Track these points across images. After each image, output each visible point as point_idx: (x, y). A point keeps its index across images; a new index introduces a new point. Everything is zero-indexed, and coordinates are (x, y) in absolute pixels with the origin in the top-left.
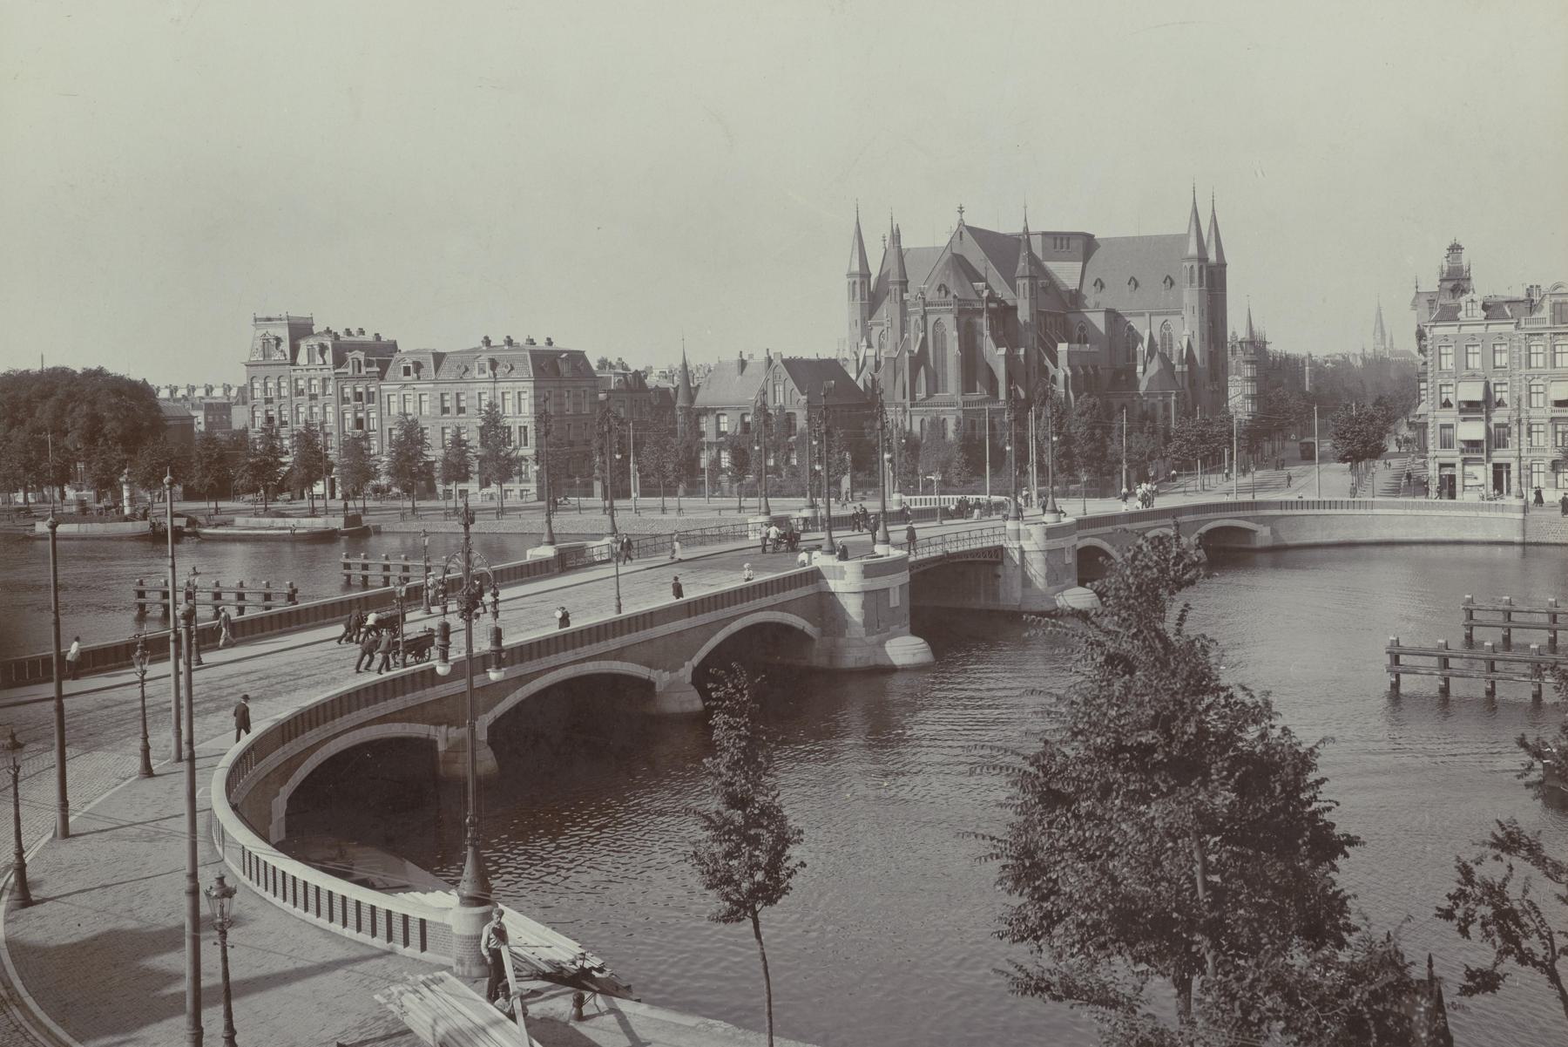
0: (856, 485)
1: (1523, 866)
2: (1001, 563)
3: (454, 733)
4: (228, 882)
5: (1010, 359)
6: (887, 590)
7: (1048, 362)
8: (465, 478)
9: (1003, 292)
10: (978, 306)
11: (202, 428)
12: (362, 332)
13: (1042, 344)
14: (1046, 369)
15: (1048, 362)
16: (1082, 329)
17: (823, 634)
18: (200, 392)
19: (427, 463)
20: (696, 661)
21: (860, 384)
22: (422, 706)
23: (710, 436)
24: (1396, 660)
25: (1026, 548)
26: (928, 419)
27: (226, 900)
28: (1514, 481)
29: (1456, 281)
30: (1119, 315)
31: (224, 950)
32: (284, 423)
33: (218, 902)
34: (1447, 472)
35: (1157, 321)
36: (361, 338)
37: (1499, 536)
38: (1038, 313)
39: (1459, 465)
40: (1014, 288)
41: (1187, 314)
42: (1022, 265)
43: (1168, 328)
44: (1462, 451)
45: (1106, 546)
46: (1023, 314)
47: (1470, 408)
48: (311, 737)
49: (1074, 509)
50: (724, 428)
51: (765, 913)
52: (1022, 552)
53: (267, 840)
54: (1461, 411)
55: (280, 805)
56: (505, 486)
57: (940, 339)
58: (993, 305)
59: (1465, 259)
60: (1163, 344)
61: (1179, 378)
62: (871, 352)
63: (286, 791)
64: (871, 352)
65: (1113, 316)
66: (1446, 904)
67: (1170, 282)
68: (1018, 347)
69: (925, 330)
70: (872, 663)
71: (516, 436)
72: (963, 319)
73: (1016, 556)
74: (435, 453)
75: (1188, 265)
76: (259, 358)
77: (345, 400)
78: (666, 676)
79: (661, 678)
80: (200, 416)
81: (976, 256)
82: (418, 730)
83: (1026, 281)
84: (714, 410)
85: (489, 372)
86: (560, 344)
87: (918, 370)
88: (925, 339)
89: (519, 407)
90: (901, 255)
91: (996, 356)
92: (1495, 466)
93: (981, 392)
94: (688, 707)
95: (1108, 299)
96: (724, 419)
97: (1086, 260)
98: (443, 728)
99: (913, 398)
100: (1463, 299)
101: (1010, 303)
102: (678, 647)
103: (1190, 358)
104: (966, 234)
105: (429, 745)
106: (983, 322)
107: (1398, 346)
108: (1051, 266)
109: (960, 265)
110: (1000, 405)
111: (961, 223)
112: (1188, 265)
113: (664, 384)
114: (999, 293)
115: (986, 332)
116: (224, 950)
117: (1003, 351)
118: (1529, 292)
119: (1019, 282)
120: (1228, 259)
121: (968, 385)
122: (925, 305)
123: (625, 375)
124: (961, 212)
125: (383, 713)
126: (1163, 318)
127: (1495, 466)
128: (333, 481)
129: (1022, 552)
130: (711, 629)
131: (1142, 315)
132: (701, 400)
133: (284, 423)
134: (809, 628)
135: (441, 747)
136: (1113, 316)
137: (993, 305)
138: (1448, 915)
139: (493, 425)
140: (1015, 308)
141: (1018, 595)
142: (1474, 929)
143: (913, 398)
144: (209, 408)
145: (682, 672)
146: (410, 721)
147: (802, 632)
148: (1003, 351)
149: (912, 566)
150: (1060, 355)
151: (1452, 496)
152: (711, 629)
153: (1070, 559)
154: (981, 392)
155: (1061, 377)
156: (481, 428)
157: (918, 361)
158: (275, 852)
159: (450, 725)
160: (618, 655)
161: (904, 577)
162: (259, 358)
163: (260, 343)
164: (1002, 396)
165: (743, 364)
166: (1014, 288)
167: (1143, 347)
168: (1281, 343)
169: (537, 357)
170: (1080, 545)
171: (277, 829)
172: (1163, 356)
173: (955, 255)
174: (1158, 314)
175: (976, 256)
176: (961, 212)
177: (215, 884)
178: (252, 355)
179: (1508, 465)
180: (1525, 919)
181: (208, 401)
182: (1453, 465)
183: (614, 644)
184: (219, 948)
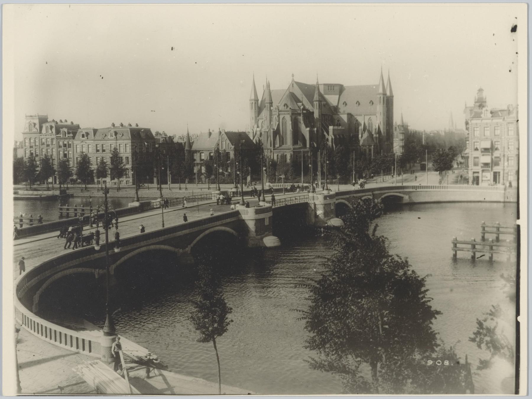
0: (253, 179)
5: (311, 132)
7: (325, 133)
8: (105, 176)
9: (308, 106)
15: (325, 133)
36: (66, 123)
39: (480, 172)
40: (313, 106)
42: (316, 97)
44: (482, 167)
45: (346, 202)
46: (316, 115)
49: (335, 188)
50: (203, 158)
54: (482, 152)
56: (121, 179)
58: (305, 112)
63: (38, 293)
69: (279, 121)
72: (293, 117)
77: (60, 147)
83: (317, 102)
89: (126, 150)
91: (305, 131)
101: (311, 111)
104: (295, 85)
106: (301, 118)
108: (327, 97)
110: (307, 150)
111: (293, 80)
112: (379, 96)
117: (308, 129)
119: (315, 103)
121: (295, 142)
123: (165, 138)
126: (368, 117)
137: (305, 112)
139: (116, 157)
140: (313, 113)
145: (187, 249)
148: (308, 129)
150: (330, 130)
154: (300, 145)
165: (210, 134)
170: (337, 202)
174: (367, 115)
182: (478, 172)
183: (162, 238)
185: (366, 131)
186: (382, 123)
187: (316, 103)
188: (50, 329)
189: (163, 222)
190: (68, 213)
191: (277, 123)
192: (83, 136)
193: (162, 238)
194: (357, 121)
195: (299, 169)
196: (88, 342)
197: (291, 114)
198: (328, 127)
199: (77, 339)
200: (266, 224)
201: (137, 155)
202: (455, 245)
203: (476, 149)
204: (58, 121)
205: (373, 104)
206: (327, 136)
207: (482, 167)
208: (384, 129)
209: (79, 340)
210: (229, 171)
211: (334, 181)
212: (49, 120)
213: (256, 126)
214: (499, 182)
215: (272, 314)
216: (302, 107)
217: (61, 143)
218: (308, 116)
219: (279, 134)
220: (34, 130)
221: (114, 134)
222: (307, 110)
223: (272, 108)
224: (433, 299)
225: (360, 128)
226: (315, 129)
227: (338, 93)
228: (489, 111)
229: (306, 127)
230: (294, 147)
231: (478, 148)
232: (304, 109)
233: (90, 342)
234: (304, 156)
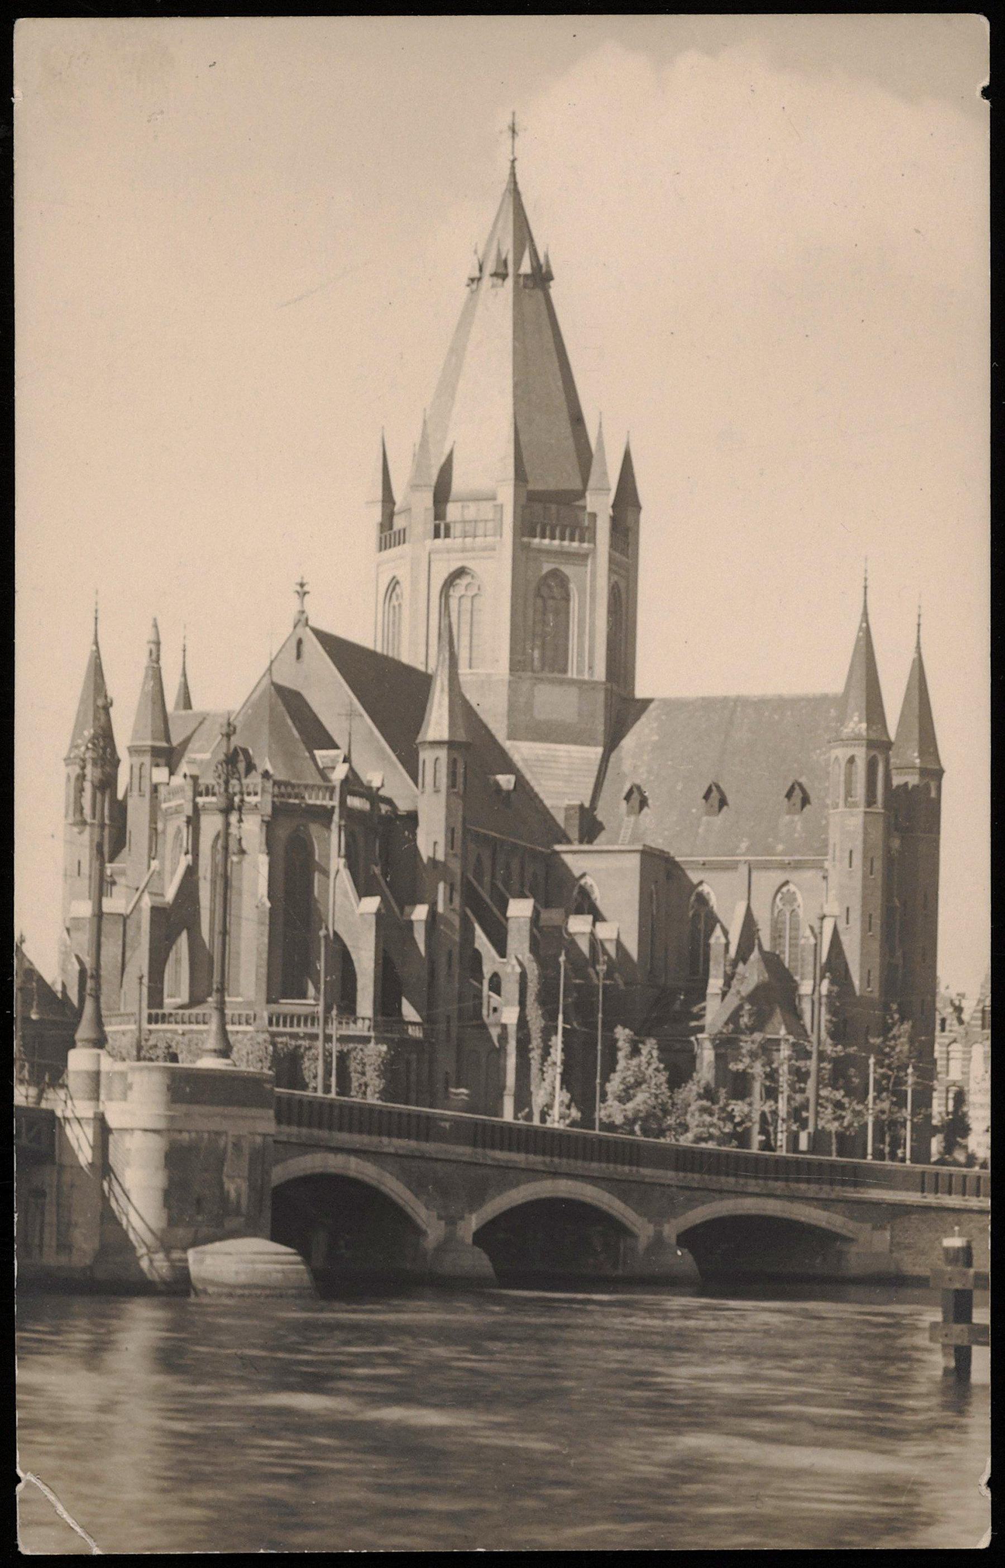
5: (391, 929)
7: (482, 941)
9: (381, 772)
10: (313, 800)
13: (471, 898)
14: (477, 958)
15: (482, 941)
25: (113, 1122)
30: (676, 865)
35: (766, 882)
38: (463, 833)
40: (411, 765)
41: (836, 867)
42: (437, 724)
43: (791, 899)
46: (431, 840)
52: (103, 1130)
58: (355, 802)
60: (777, 935)
65: (663, 878)
67: (799, 796)
68: (415, 902)
69: (195, 851)
72: (282, 833)
73: (80, 1141)
75: (841, 753)
81: (332, 698)
83: (443, 754)
87: (171, 939)
88: (191, 871)
91: (352, 914)
93: (313, 1001)
95: (655, 827)
97: (612, 742)
99: (156, 997)
101: (403, 806)
103: (835, 966)
104: (313, 647)
106: (331, 847)
108: (522, 751)
109: (292, 712)
110: (361, 1028)
111: (302, 620)
112: (841, 753)
114: (373, 778)
115: (337, 863)
117: (372, 904)
119: (426, 756)
122: (197, 793)
124: (303, 594)
126: (777, 877)
129: (103, 1130)
131: (730, 867)
136: (663, 878)
137: (355, 802)
140: (412, 818)
143: (156, 997)
148: (372, 904)
150: (512, 926)
154: (313, 1001)
155: (509, 970)
157: (173, 920)
164: (365, 1005)
166: (411, 765)
172: (772, 961)
173: (280, 690)
174: (766, 866)
176: (303, 594)
185: (755, 955)
186: (856, 915)
187: (434, 761)
189: (600, 426)
191: (185, 861)
194: (702, 900)
197: (268, 810)
198: (504, 907)
205: (805, 801)
206: (490, 962)
208: (864, 954)
215: (477, 274)
216: (340, 773)
218: (381, 842)
219: (192, 925)
222: (372, 795)
224: (394, 578)
225: (717, 938)
226: (420, 913)
227: (600, 727)
229: (363, 891)
230: (274, 1008)
232: (352, 784)
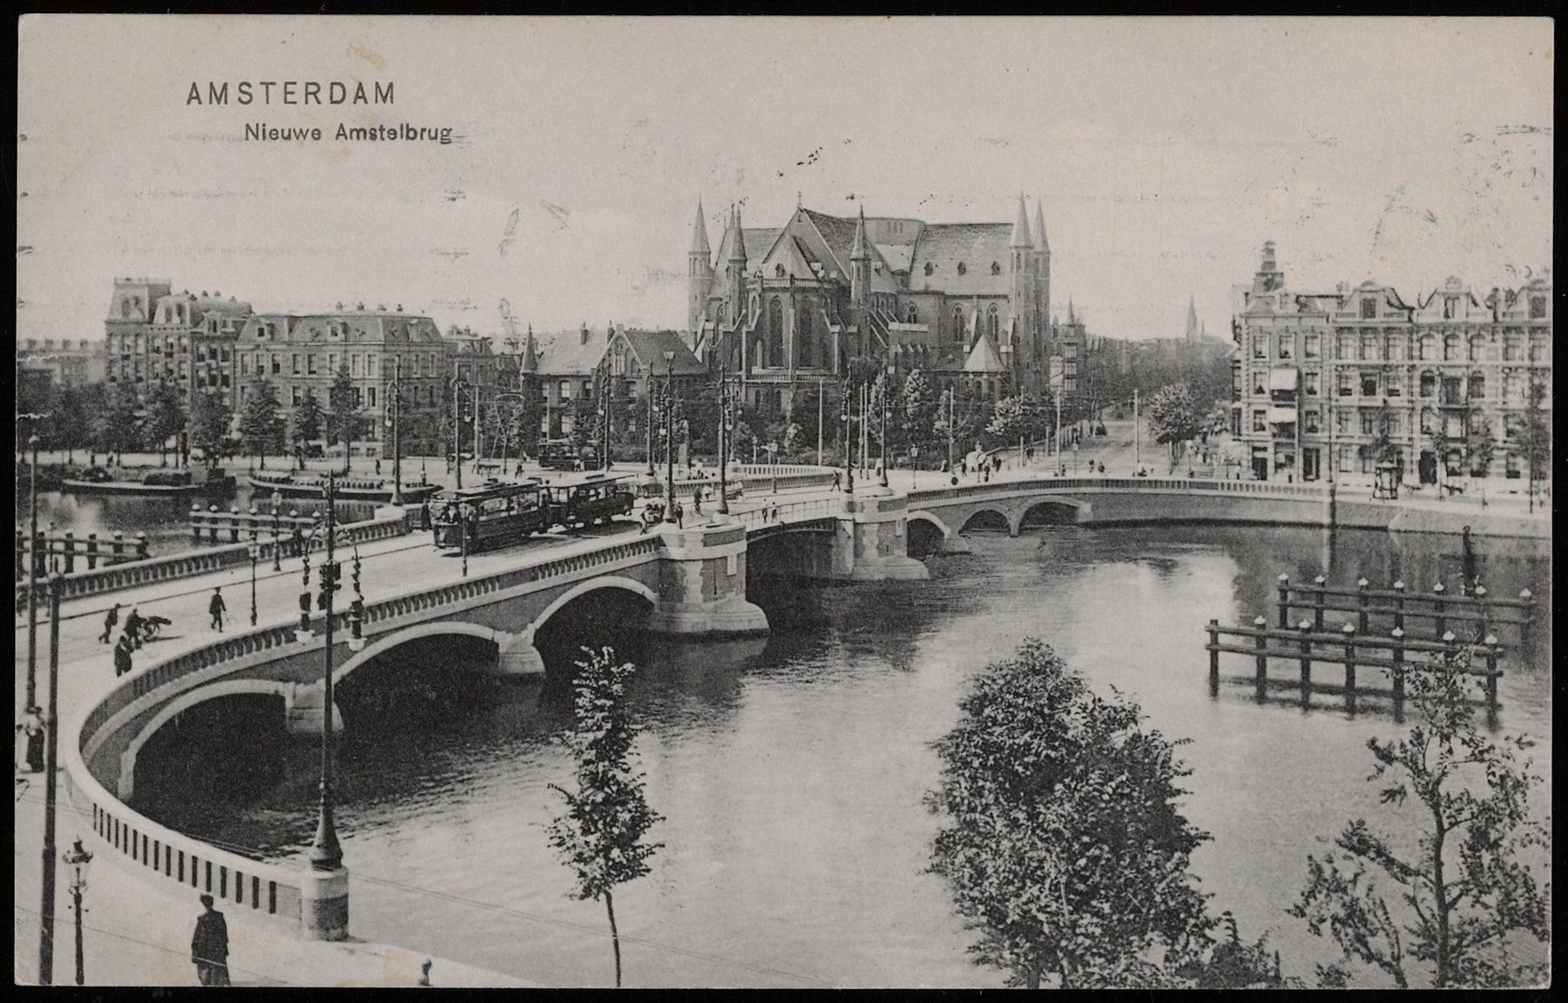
0: (693, 452)
1: (1374, 869)
2: (835, 533)
3: (302, 689)
4: (85, 847)
6: (725, 558)
8: (316, 436)
11: (1008, 973)
12: (218, 294)
16: (912, 309)
17: (662, 597)
18: (58, 346)
19: (277, 421)
20: (539, 623)
21: (698, 355)
22: (271, 663)
23: (552, 402)
24: (1215, 640)
26: (763, 391)
27: (82, 865)
28: (1324, 466)
29: (1269, 279)
31: (78, 914)
32: (139, 379)
33: (74, 866)
34: (1259, 455)
36: (219, 300)
37: (1308, 517)
39: (1271, 450)
44: (1274, 435)
45: (934, 519)
47: (1283, 397)
48: (163, 691)
49: (904, 481)
50: (565, 394)
51: (617, 889)
53: (116, 795)
54: (1274, 398)
55: (129, 760)
56: (353, 444)
57: (777, 320)
59: (1279, 258)
61: (1004, 357)
62: (710, 326)
63: (136, 744)
64: (710, 326)
66: (1300, 902)
67: (996, 269)
70: (709, 628)
71: (366, 399)
74: (286, 412)
76: (119, 316)
77: (201, 358)
78: (510, 637)
79: (504, 640)
80: (57, 369)
82: (266, 686)
84: (556, 377)
85: (341, 336)
86: (408, 311)
87: (755, 344)
89: (368, 373)
90: (740, 233)
92: (1306, 450)
94: (529, 669)
96: (564, 386)
98: (292, 685)
100: (1276, 293)
102: (523, 608)
105: (278, 699)
107: (1209, 331)
113: (508, 350)
116: (78, 914)
118: (1339, 288)
120: (1052, 247)
121: (803, 361)
123: (472, 342)
125: (232, 669)
127: (1306, 450)
128: (185, 435)
130: (554, 592)
132: (543, 370)
133: (139, 379)
134: (650, 595)
135: (289, 704)
138: (1300, 912)
139: (343, 388)
141: (850, 565)
142: (1326, 927)
144: (67, 362)
145: (524, 634)
146: (259, 677)
147: (642, 597)
149: (750, 535)
151: (1264, 478)
152: (554, 592)
153: (901, 531)
156: (332, 389)
158: (126, 808)
159: (298, 682)
160: (464, 615)
161: (742, 546)
162: (119, 316)
163: (119, 302)
165: (586, 334)
167: (971, 327)
168: (1099, 327)
169: (389, 322)
170: (910, 517)
171: (126, 784)
175: (816, 240)
177: (72, 848)
178: (112, 312)
179: (1318, 451)
180: (1370, 917)
181: (65, 354)
182: (1265, 449)
183: (460, 604)
184: (73, 911)
188: (195, 859)
190: (214, 531)
192: (261, 333)
193: (460, 604)
195: (819, 430)
196: (267, 888)
199: (256, 881)
200: (926, 575)
201: (400, 382)
202: (1214, 635)
203: (1260, 391)
204: (198, 295)
207: (1274, 435)
209: (244, 880)
210: (633, 428)
211: (900, 460)
212: (173, 292)
213: (703, 317)
214: (1318, 477)
217: (203, 349)
220: (135, 315)
221: (340, 330)
223: (744, 274)
228: (1293, 298)
231: (1266, 388)
233: (273, 885)
234: (825, 393)
